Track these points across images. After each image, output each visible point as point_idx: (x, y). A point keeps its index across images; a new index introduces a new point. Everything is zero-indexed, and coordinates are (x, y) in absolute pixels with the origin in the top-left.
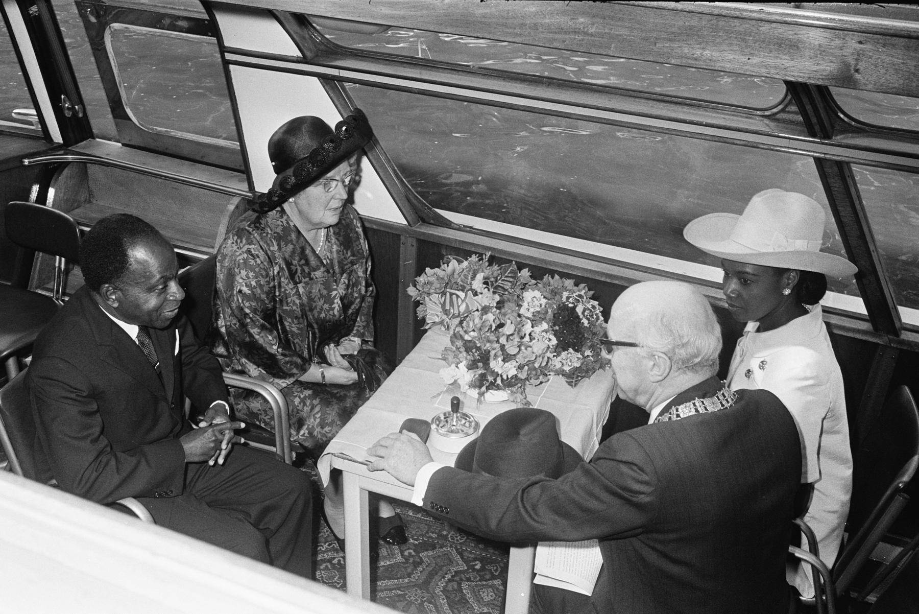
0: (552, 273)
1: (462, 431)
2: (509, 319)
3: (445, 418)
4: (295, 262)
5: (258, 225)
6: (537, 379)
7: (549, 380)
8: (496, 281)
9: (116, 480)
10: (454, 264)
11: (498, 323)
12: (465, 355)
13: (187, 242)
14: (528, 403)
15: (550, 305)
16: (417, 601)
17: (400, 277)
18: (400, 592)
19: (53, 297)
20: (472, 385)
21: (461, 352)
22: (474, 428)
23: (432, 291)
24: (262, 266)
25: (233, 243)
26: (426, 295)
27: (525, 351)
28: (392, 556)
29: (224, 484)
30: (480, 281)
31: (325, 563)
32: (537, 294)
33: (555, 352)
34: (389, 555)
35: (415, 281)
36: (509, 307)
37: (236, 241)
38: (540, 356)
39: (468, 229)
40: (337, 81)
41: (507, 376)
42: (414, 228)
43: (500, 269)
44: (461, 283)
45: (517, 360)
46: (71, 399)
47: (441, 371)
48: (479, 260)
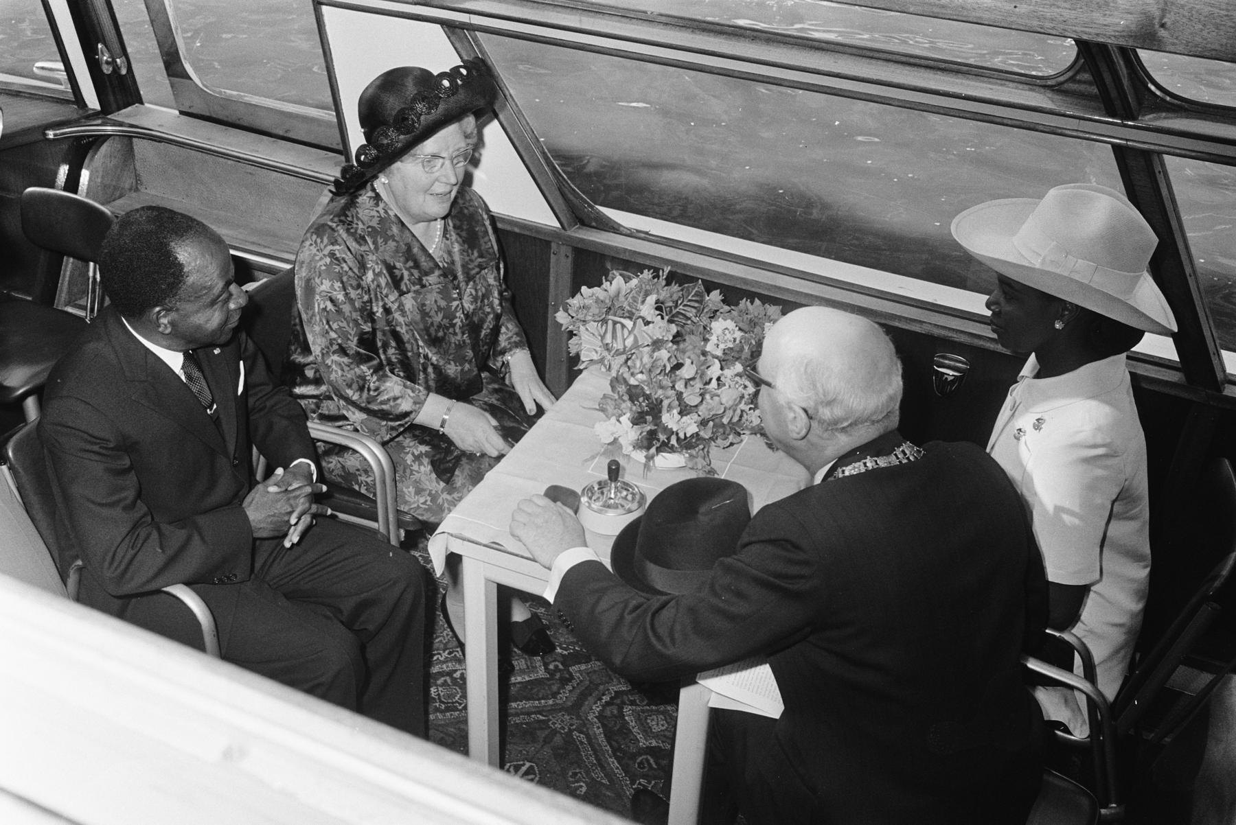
0: (751, 296)
1: (623, 506)
2: (689, 358)
3: (599, 489)
4: (398, 265)
5: (343, 218)
6: (725, 439)
7: (742, 441)
8: (676, 306)
9: (160, 559)
10: (618, 281)
11: (675, 363)
12: (629, 405)
13: (265, 247)
14: (712, 471)
15: (748, 341)
16: (564, 729)
17: (550, 299)
18: (541, 718)
19: (86, 317)
20: (638, 446)
21: (624, 401)
22: (639, 502)
23: (589, 318)
24: (350, 273)
25: (311, 245)
26: (582, 323)
27: (710, 401)
28: (528, 670)
29: (307, 570)
30: (651, 305)
31: (443, 676)
32: (730, 324)
33: (752, 403)
34: (528, 668)
35: (567, 303)
36: (691, 341)
37: (316, 242)
38: (730, 409)
39: (643, 235)
40: (467, 30)
41: (685, 434)
42: (569, 233)
43: (682, 290)
44: (628, 308)
45: (700, 413)
46: (94, 452)
47: (597, 425)
48: (654, 278)
